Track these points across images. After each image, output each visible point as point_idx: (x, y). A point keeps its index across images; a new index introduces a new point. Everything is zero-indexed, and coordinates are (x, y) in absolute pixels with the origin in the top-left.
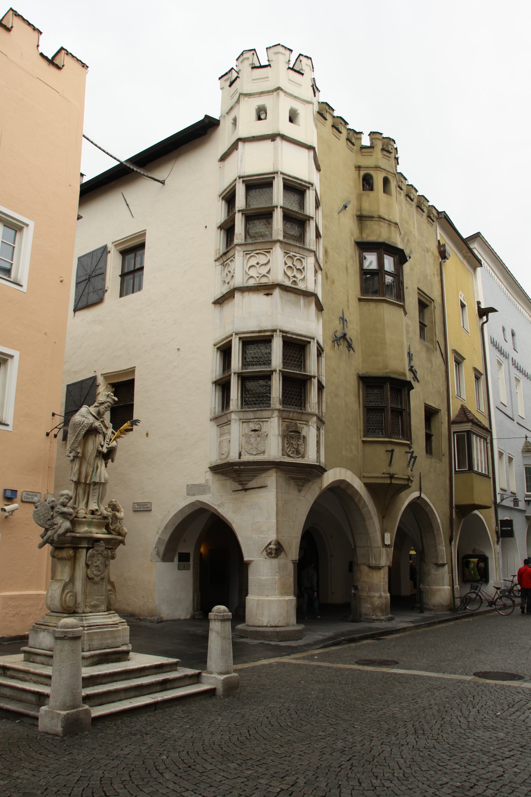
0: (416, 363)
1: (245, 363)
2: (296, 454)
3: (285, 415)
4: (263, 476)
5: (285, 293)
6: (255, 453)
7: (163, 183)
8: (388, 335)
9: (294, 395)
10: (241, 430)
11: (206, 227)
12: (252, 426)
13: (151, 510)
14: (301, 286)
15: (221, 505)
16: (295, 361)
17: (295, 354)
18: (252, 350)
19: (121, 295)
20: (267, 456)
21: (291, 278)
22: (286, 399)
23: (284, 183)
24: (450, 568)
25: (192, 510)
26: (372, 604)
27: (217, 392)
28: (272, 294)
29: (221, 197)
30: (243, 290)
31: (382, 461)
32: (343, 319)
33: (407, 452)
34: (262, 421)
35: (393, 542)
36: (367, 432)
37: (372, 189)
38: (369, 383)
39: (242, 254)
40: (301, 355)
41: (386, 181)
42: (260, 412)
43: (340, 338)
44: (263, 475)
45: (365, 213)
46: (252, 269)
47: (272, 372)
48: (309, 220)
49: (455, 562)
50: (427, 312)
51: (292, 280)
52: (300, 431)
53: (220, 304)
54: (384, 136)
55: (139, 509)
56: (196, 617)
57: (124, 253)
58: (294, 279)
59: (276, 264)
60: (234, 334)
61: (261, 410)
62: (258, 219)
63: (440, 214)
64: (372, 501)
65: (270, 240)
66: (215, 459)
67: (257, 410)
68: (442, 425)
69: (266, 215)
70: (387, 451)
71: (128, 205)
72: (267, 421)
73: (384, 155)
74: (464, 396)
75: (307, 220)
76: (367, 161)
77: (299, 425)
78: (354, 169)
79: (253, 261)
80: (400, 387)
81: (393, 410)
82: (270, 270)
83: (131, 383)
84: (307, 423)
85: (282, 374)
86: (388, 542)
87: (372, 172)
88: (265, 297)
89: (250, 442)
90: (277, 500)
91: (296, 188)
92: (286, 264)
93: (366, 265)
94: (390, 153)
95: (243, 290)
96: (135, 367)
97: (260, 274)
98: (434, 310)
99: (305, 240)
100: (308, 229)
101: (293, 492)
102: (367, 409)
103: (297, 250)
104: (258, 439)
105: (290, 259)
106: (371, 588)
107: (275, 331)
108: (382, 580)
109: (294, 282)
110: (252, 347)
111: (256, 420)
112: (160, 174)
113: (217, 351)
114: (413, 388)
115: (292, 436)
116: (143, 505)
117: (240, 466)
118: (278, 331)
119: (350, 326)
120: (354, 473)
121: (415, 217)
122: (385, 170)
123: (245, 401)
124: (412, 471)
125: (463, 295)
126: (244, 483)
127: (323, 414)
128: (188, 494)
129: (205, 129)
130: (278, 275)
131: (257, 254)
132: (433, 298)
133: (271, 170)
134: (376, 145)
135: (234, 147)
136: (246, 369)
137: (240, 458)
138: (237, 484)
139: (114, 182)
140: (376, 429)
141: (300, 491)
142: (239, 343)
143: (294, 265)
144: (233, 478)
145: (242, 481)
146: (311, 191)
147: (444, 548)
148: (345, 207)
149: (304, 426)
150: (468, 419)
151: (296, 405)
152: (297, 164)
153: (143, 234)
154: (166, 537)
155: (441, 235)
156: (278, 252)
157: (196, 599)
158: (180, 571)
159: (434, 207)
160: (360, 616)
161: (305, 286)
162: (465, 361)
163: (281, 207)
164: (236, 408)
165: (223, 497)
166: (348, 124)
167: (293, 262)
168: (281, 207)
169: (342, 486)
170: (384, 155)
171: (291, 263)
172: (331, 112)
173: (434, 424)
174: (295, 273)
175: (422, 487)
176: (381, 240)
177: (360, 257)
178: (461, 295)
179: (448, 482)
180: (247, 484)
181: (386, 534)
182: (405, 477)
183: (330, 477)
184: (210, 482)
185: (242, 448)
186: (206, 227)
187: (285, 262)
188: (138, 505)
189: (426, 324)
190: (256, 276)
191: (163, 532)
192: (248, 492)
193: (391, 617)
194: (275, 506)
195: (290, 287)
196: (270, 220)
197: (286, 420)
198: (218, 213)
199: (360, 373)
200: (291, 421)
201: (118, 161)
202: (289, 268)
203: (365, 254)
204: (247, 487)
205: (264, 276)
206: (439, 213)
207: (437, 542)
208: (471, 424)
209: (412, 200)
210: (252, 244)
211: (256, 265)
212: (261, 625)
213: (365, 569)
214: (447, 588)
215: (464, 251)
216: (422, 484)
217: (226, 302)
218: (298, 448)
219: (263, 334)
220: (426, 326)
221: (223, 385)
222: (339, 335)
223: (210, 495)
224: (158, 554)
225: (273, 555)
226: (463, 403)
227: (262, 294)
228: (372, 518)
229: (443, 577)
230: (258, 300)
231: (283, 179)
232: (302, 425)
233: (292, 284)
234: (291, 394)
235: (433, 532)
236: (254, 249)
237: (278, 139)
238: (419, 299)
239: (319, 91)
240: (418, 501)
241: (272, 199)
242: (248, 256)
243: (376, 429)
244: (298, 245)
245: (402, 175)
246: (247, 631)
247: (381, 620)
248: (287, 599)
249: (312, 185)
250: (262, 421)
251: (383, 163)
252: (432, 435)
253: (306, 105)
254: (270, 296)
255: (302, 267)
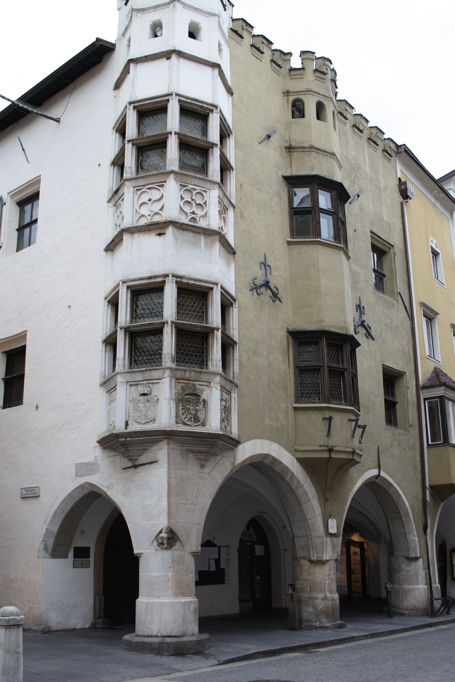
0: (369, 318)
1: (134, 314)
2: (194, 422)
3: (179, 374)
4: (154, 449)
5: (181, 231)
6: (143, 421)
7: (57, 121)
8: (323, 282)
9: (194, 351)
10: (128, 395)
11: (99, 165)
12: (142, 389)
13: (38, 496)
14: (202, 223)
15: (110, 486)
16: (194, 311)
17: (194, 303)
18: (143, 301)
19: (17, 251)
20: (158, 425)
21: (189, 214)
22: (181, 356)
23: (181, 106)
24: (426, 562)
25: (82, 495)
26: (314, 607)
27: (107, 353)
28: (165, 234)
29: (115, 129)
30: (132, 231)
31: (314, 431)
32: (265, 265)
33: (350, 420)
34: (153, 383)
35: (342, 530)
36: (300, 396)
37: (303, 117)
38: (301, 339)
39: (132, 190)
40: (203, 304)
41: (320, 108)
42: (149, 372)
43: (261, 286)
44: (154, 448)
45: (294, 144)
46: (144, 207)
47: (163, 324)
48: (212, 148)
49: (433, 555)
50: (386, 260)
51: (190, 217)
52: (200, 394)
53: (112, 250)
54: (318, 55)
55: (26, 496)
56: (98, 626)
57: (22, 204)
58: (193, 216)
59: (170, 199)
60: (121, 283)
61: (150, 370)
62: (152, 150)
63: (399, 148)
64: (309, 480)
65: (165, 171)
66: (102, 430)
67: (146, 370)
68: (408, 391)
69: (160, 144)
70: (324, 419)
71: (23, 150)
72: (159, 383)
73: (317, 76)
74: (439, 356)
75: (210, 147)
76: (296, 85)
77: (198, 387)
78: (281, 95)
79: (145, 198)
80: (342, 345)
81: (332, 371)
82: (163, 206)
83: (22, 351)
84: (208, 384)
85: (175, 327)
86: (333, 529)
87: (302, 97)
88: (158, 236)
89: (139, 409)
90: (169, 478)
91: (196, 112)
92: (182, 198)
93: (296, 202)
94: (325, 74)
95: (132, 231)
96: (26, 331)
97: (152, 212)
98: (394, 257)
99: (208, 170)
100: (211, 158)
101: (192, 468)
102: (300, 370)
103: (197, 182)
104: (148, 404)
105: (187, 193)
106: (313, 588)
107: (167, 276)
108: (327, 578)
109: (193, 219)
110: (144, 297)
111: (146, 382)
112: (54, 112)
113: (108, 306)
114: (359, 345)
115: (189, 399)
116: (31, 491)
117: (126, 438)
118: (170, 276)
119: (274, 272)
120: (282, 446)
121: (366, 150)
122: (319, 94)
123: (135, 361)
124: (360, 443)
125: (434, 242)
126: (134, 458)
127: (236, 375)
128: (77, 475)
129: (96, 56)
130: (172, 212)
131: (149, 189)
132: (392, 243)
133: (165, 92)
134: (308, 66)
135: (126, 71)
136: (136, 322)
137: (126, 428)
138: (126, 460)
139: (11, 127)
140: (311, 393)
141: (203, 466)
142: (127, 292)
143: (193, 200)
144: (121, 453)
145: (131, 456)
146: (214, 114)
147: (416, 538)
148: (269, 137)
149: (205, 387)
150: (441, 382)
151: (196, 364)
152: (199, 85)
153: (37, 181)
154: (55, 528)
155: (400, 170)
156: (172, 185)
157: (97, 603)
158: (76, 569)
159: (392, 140)
160: (301, 622)
161: (207, 223)
162: (438, 316)
163: (176, 133)
164: (122, 369)
165: (112, 477)
166: (272, 43)
167: (192, 196)
168: (176, 133)
169: (267, 462)
170: (317, 76)
171: (190, 197)
172: (249, 29)
173: (399, 390)
174: (194, 208)
175: (381, 464)
176: (314, 173)
177: (289, 194)
178: (432, 241)
179: (418, 458)
180: (137, 459)
181: (330, 521)
182: (349, 450)
183: (247, 451)
184: (99, 459)
185: (129, 417)
186: (99, 165)
187: (181, 196)
188: (26, 491)
189: (385, 274)
190: (148, 214)
191: (51, 522)
192: (139, 469)
193: (341, 624)
194: (166, 485)
195: (187, 225)
196: (164, 150)
197: (181, 381)
198: (110, 145)
199: (289, 328)
200: (187, 382)
201: (9, 100)
202: (186, 203)
203: (295, 190)
204: (137, 463)
205: (157, 213)
206: (398, 147)
207: (407, 530)
208: (443, 388)
209: (361, 131)
210: (143, 177)
211: (148, 202)
212: (150, 634)
213: (305, 563)
214: (422, 587)
215: (435, 192)
216: (381, 461)
217: (116, 248)
218: (196, 414)
219: (153, 280)
220: (385, 276)
221: (110, 342)
222: (259, 282)
223: (99, 475)
224: (46, 549)
225: (165, 546)
226: (437, 365)
227: (154, 234)
228: (309, 501)
229: (417, 574)
230: (150, 241)
231: (179, 101)
232: (202, 387)
233: (189, 221)
234: (189, 351)
235: (401, 518)
236: (146, 183)
237: (174, 57)
238: (372, 242)
239: (233, 6)
240: (378, 481)
241: (166, 126)
242: (139, 192)
243: (311, 393)
244: (201, 177)
245: (347, 102)
246: (132, 642)
247: (326, 628)
248: (183, 601)
249: (216, 107)
250: (153, 383)
251: (315, 85)
252: (397, 403)
253: (210, 17)
254: (162, 236)
255: (204, 201)
